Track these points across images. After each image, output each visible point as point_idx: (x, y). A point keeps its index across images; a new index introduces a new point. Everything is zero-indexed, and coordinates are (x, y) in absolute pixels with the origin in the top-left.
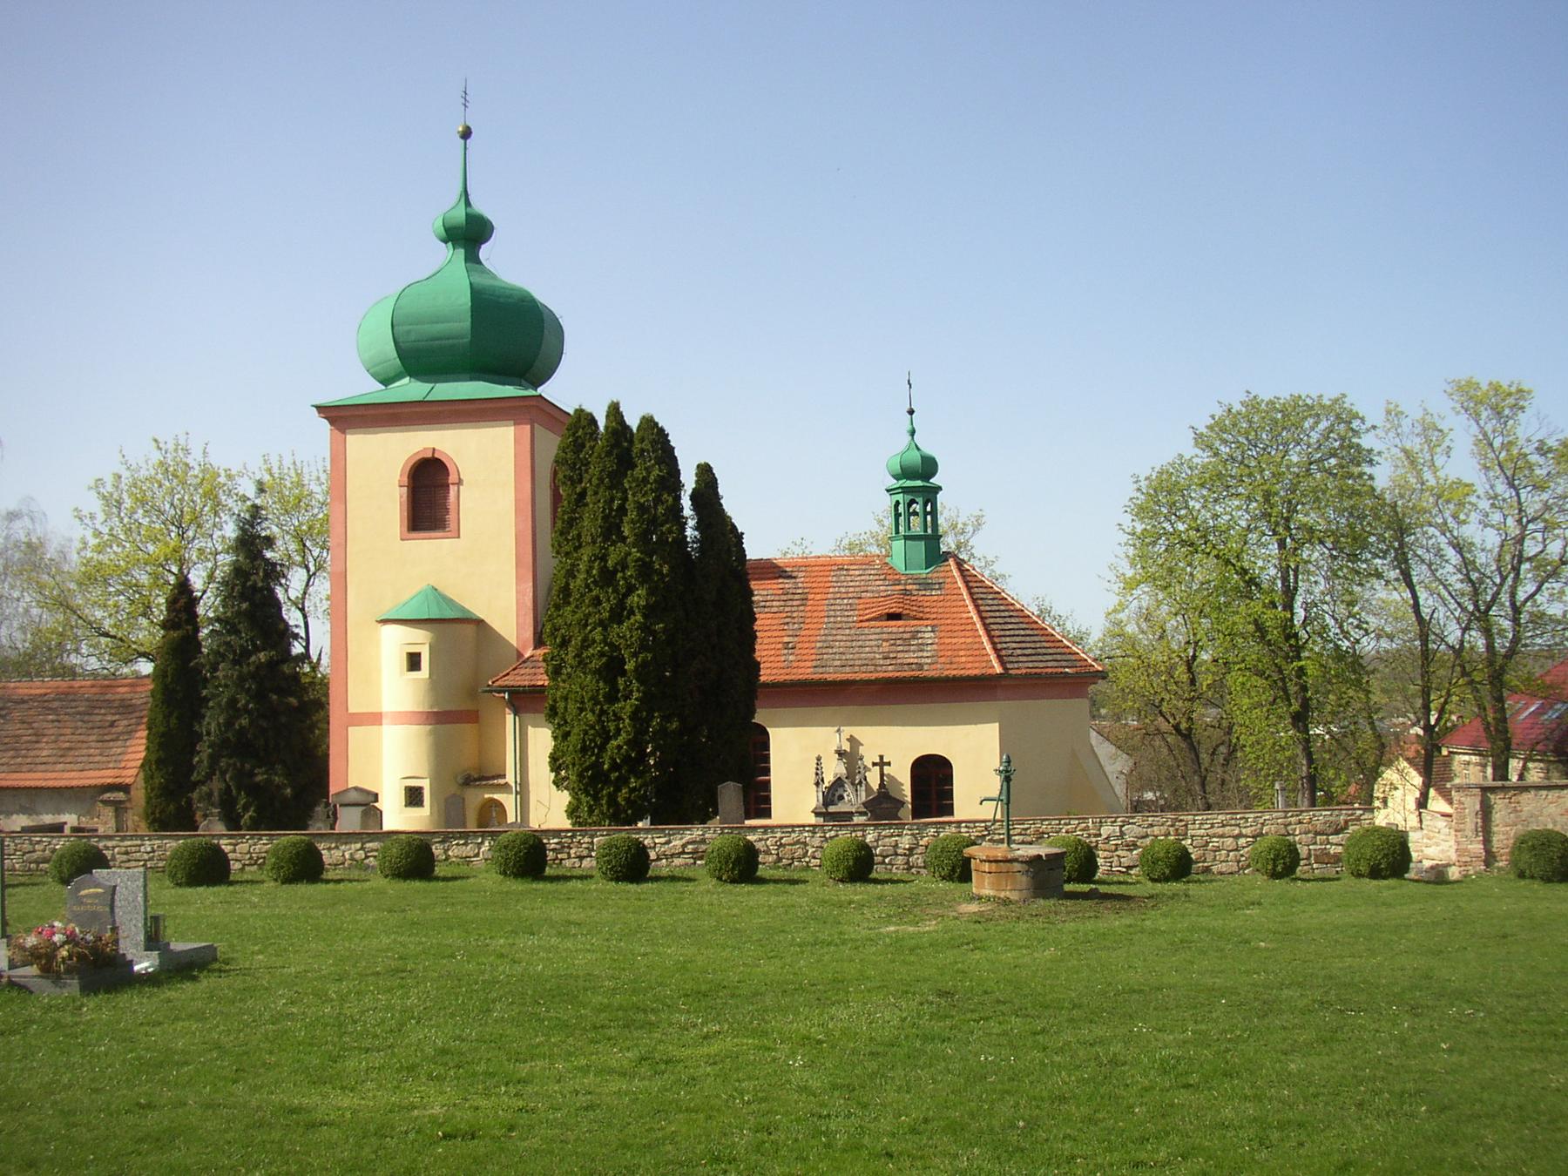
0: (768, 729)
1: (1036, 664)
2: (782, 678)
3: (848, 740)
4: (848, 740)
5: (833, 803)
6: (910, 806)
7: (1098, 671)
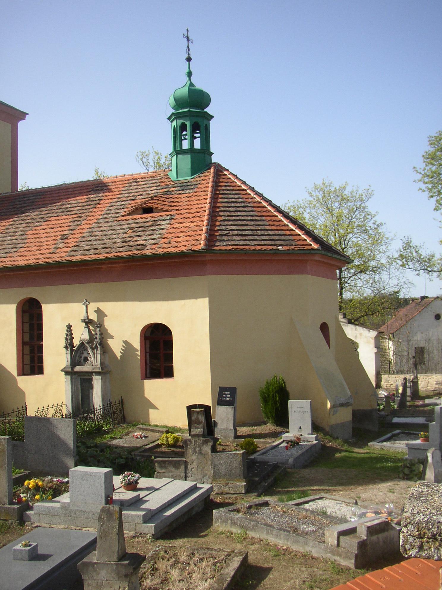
0: (42, 305)
1: (248, 243)
2: (41, 261)
3: (95, 311)
4: (95, 311)
5: (79, 364)
6: (139, 358)
7: (313, 249)
